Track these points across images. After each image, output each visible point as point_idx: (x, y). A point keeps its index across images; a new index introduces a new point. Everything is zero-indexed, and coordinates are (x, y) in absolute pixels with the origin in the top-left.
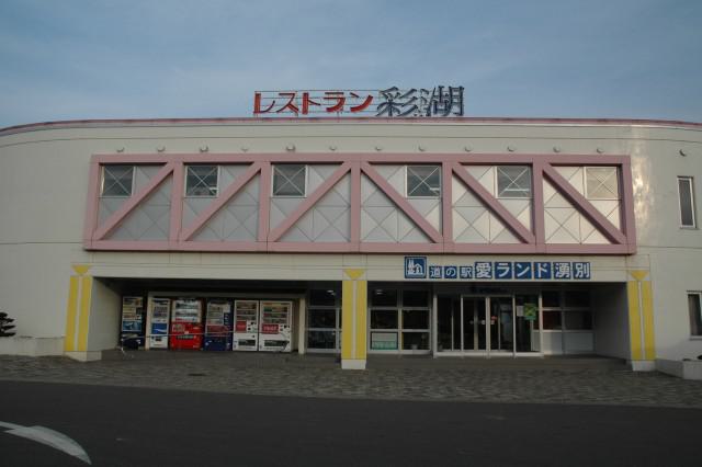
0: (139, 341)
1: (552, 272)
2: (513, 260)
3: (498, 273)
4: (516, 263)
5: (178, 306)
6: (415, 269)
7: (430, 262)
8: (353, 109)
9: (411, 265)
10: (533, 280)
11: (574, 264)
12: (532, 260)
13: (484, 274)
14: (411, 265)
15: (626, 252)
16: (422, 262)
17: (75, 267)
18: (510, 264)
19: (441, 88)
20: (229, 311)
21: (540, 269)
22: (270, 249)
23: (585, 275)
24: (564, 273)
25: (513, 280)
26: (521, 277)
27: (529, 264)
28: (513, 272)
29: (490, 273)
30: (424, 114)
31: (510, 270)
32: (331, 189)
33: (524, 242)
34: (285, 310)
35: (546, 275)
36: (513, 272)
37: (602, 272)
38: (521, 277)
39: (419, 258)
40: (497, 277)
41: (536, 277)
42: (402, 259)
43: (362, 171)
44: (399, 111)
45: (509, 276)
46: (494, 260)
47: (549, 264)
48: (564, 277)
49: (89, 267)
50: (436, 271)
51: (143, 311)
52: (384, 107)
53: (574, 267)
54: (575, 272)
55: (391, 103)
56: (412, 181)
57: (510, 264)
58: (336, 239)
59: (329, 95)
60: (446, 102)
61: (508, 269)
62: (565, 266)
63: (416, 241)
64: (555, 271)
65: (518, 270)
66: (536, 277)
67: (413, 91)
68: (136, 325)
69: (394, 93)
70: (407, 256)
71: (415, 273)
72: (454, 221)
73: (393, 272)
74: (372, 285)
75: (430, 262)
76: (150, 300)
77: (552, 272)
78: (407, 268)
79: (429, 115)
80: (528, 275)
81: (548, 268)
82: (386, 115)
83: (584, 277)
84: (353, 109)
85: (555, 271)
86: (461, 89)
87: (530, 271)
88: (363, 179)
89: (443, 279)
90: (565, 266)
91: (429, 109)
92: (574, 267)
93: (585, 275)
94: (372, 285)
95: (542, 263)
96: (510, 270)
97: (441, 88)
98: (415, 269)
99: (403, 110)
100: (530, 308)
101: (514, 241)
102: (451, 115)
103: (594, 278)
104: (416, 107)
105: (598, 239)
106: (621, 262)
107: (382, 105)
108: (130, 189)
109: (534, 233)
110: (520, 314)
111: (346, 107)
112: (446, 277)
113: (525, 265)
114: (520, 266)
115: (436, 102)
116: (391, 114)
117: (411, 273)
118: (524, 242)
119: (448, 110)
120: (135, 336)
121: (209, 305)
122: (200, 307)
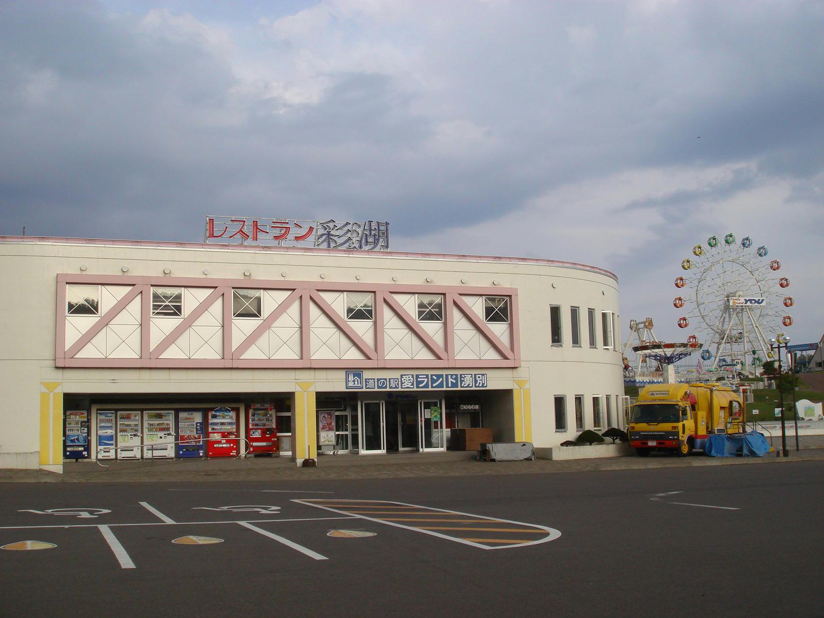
0: (85, 453)
1: (459, 382)
2: (430, 373)
3: (418, 383)
4: (432, 375)
5: (214, 417)
6: (354, 381)
7: (366, 375)
8: (297, 238)
9: (351, 378)
10: (445, 389)
11: (475, 375)
12: (444, 373)
13: (408, 385)
14: (351, 378)
15: (513, 366)
16: (359, 376)
17: (42, 383)
18: (427, 376)
19: (370, 222)
20: (200, 421)
21: (450, 380)
22: (235, 366)
23: (483, 384)
24: (468, 383)
25: (430, 389)
26: (422, 387)
27: (441, 376)
28: (430, 383)
29: (413, 384)
30: (357, 245)
31: (428, 381)
32: (203, 307)
33: (440, 358)
34: (233, 419)
35: (454, 385)
36: (430, 383)
37: (495, 382)
38: (422, 387)
39: (357, 372)
40: (418, 387)
41: (447, 386)
42: (342, 374)
43: (301, 297)
44: (336, 242)
45: (427, 386)
46: (415, 373)
47: (457, 375)
48: (468, 386)
49: (60, 384)
50: (372, 381)
51: (87, 424)
52: (324, 237)
53: (475, 378)
54: (476, 381)
55: (329, 234)
56: (489, 311)
57: (427, 376)
58: (289, 354)
59: (276, 224)
60: (375, 235)
61: (426, 380)
62: (468, 377)
63: (353, 355)
64: (461, 382)
65: (433, 381)
66: (447, 386)
67: (348, 224)
68: (81, 439)
69: (331, 225)
70: (348, 370)
71: (354, 385)
72: (311, 335)
73: (337, 384)
74: (319, 395)
75: (366, 375)
76: (146, 417)
77: (459, 382)
78: (347, 381)
79: (361, 247)
80: (441, 385)
81: (456, 379)
82: (325, 245)
83: (483, 386)
84: (297, 238)
85: (461, 382)
86: (387, 224)
87: (442, 381)
88: (220, 300)
89: (376, 390)
90: (468, 377)
91: (360, 241)
92: (475, 378)
93: (483, 384)
94: (319, 395)
95: (452, 375)
96: (428, 381)
97: (370, 222)
98: (354, 381)
99: (340, 241)
100: (435, 411)
101: (429, 356)
102: (379, 247)
103: (491, 386)
104: (350, 239)
105: (491, 355)
106: (509, 373)
107: (322, 235)
108: (489, 320)
109: (376, 350)
110: (428, 416)
111: (291, 236)
112: (379, 387)
113: (439, 376)
114: (435, 378)
115: (366, 236)
116: (329, 246)
117: (351, 384)
118: (505, 358)
119: (376, 243)
120: (81, 449)
121: (786, 422)
122: (234, 417)
